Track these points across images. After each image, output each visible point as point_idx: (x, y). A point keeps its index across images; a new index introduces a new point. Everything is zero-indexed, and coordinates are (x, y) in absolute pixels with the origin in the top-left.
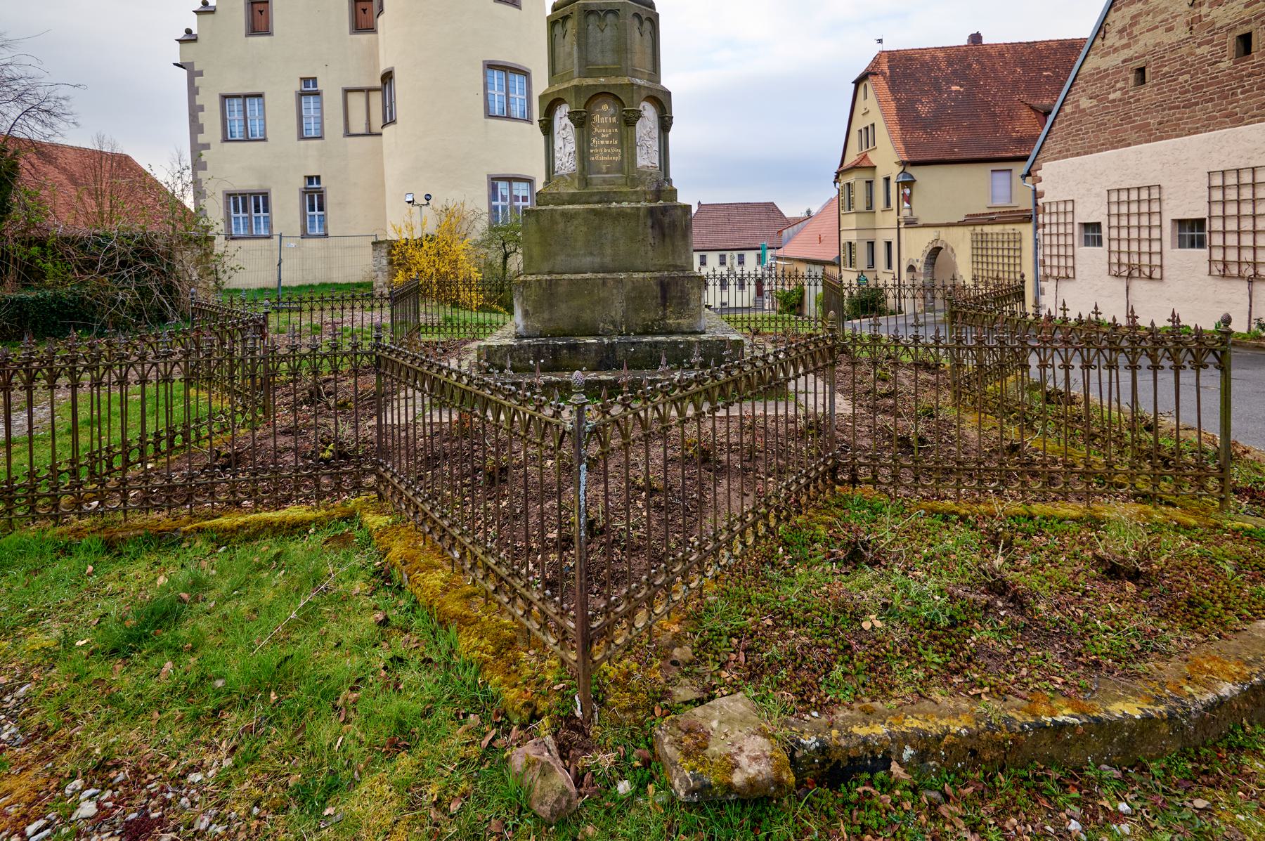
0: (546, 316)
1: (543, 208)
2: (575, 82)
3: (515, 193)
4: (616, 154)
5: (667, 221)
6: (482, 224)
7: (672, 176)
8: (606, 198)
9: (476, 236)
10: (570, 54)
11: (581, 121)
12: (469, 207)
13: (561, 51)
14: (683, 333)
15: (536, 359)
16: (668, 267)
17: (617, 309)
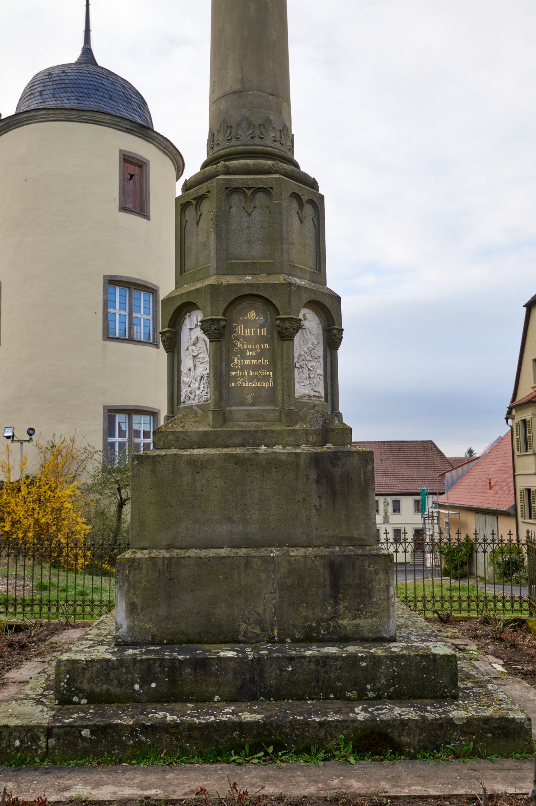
0: (162, 611)
1: (163, 452)
2: (212, 280)
3: (135, 427)
4: (266, 379)
5: (342, 472)
6: (95, 464)
7: (342, 409)
8: (251, 439)
9: (86, 479)
10: (205, 245)
11: (218, 333)
12: (79, 444)
13: (194, 241)
14: (363, 640)
15: (144, 683)
16: (340, 541)
17: (266, 603)
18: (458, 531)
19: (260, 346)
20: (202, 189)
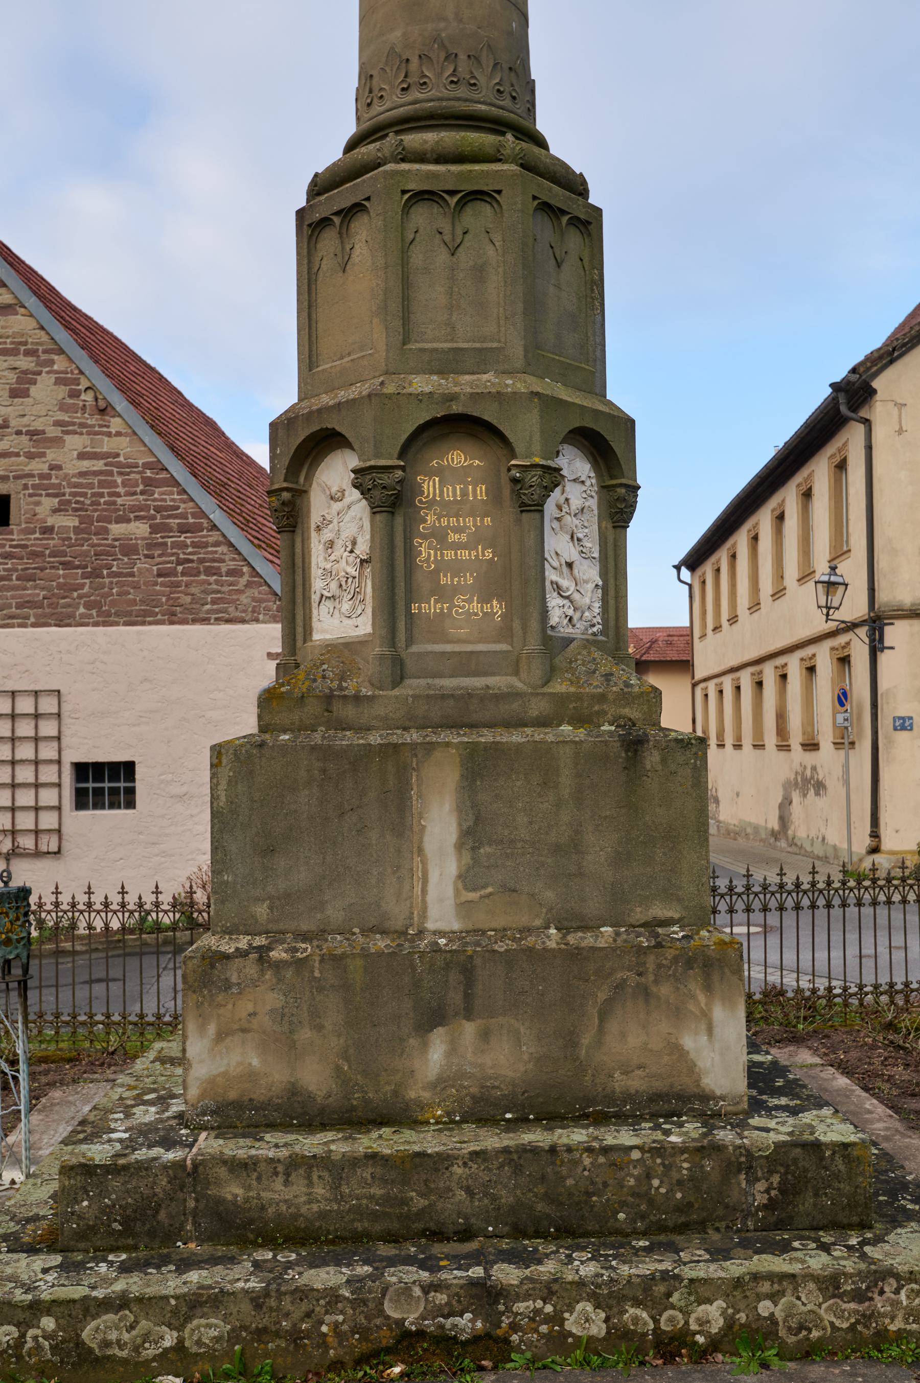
11: (390, 498)
18: (781, 869)
19: (475, 521)
20: (344, 197)
